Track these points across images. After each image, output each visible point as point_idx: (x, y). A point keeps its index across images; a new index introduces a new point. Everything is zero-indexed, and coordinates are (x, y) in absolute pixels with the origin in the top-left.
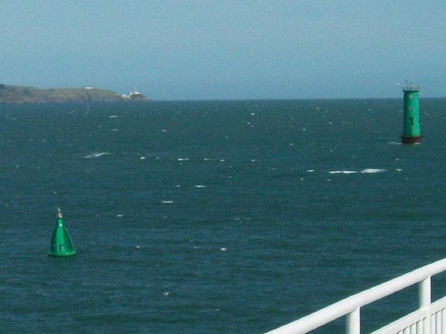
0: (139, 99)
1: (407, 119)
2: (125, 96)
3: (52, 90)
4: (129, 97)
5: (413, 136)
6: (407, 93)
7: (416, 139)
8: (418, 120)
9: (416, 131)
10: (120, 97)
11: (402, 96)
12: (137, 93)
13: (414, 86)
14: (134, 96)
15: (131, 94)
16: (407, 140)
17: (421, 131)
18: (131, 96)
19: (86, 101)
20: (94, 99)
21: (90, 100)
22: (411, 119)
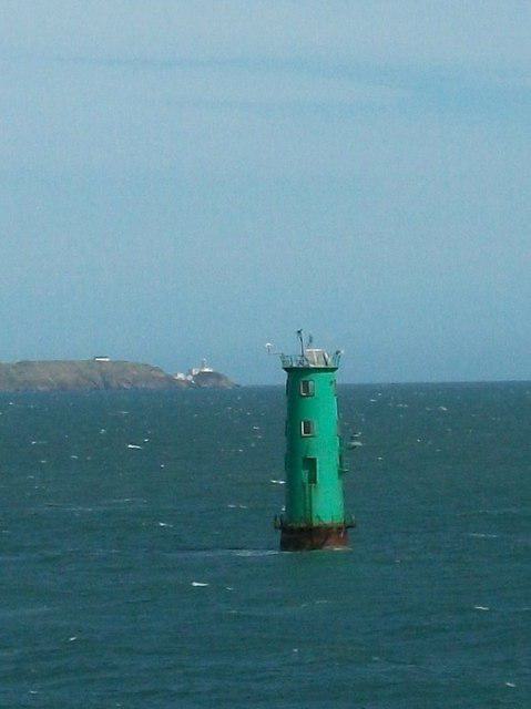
0: (212, 382)
1: (299, 464)
2: (181, 376)
3: (25, 364)
4: (190, 378)
5: (316, 523)
6: (298, 375)
7: (341, 531)
8: (335, 460)
9: (328, 504)
10: (171, 380)
11: (282, 379)
12: (207, 370)
13: (315, 355)
14: (202, 376)
15: (195, 372)
16: (300, 536)
17: (347, 505)
18: (196, 377)
19: (97, 389)
20: (114, 384)
21: (107, 385)
22: (311, 464)
